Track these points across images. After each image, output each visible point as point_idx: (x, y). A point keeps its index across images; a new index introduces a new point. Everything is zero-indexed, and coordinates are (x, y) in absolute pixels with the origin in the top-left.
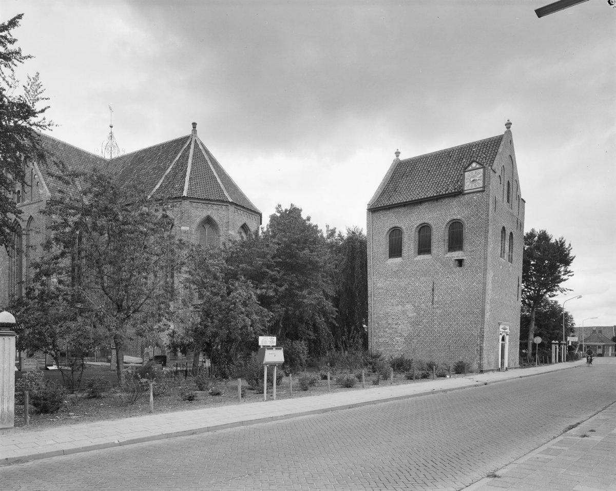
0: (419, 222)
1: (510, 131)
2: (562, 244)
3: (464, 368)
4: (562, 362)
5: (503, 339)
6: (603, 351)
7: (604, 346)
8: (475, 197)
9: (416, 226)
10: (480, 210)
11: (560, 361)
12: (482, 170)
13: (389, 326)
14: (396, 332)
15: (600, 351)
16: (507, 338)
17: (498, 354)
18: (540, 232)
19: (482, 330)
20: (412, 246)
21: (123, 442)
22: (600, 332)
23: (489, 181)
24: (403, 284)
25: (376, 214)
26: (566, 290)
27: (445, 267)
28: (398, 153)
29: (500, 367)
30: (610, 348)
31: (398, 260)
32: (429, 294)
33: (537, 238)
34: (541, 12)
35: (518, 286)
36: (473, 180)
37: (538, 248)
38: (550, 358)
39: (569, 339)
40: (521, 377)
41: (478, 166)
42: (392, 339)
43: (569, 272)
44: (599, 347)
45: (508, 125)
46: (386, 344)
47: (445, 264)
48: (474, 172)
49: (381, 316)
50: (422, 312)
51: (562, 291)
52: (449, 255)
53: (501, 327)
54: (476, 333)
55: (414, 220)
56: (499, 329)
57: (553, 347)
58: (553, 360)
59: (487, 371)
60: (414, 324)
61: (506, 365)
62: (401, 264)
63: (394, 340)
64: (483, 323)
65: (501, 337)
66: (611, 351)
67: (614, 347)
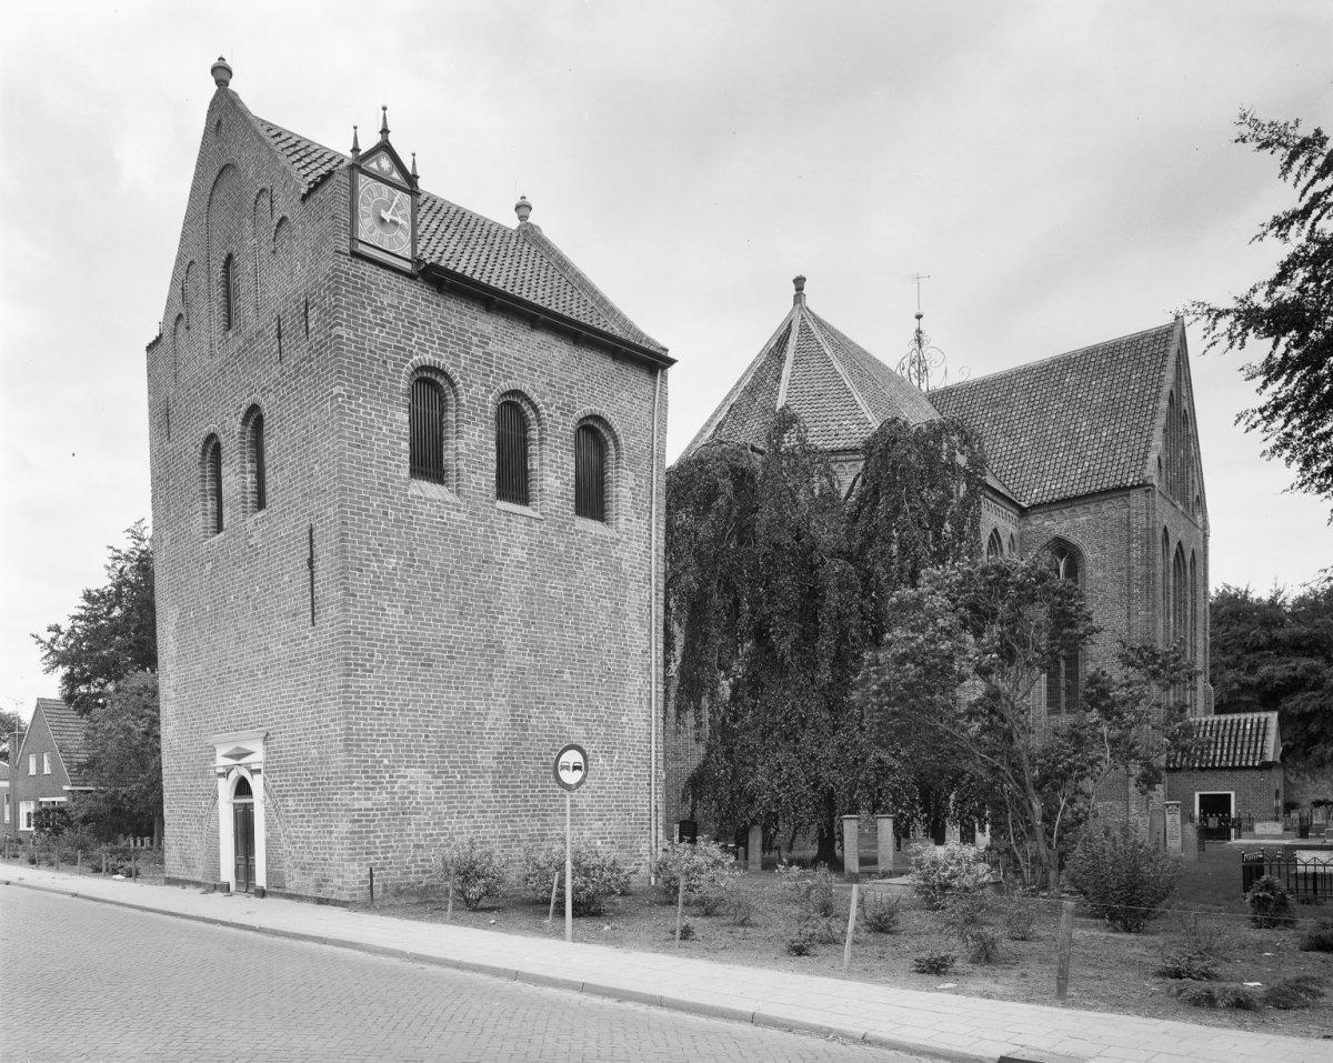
4: (563, 939)
5: (243, 788)
16: (256, 784)
29: (227, 873)
45: (222, 72)
61: (261, 880)
65: (226, 788)
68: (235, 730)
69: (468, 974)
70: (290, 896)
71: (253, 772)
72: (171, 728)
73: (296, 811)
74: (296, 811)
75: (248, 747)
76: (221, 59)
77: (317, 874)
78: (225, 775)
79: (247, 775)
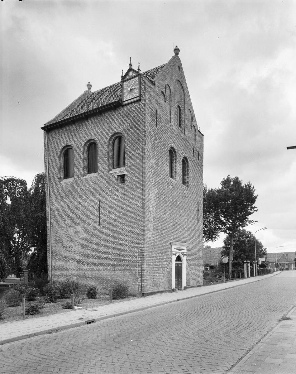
0: (87, 139)
1: (178, 59)
2: (250, 187)
3: (228, 278)
4: (254, 276)
5: (179, 259)
6: (289, 267)
7: (289, 263)
8: (133, 108)
9: (84, 143)
10: (137, 121)
11: (252, 275)
12: (137, 78)
13: (64, 249)
14: (70, 255)
15: (287, 267)
16: (184, 259)
17: (171, 275)
18: (234, 178)
19: (143, 249)
20: (81, 165)
21: (158, 304)
22: (287, 255)
23: (145, 90)
24: (74, 204)
25: (51, 134)
26: (253, 222)
27: (109, 184)
28: (89, 86)
29: (174, 286)
30: (293, 264)
31: (71, 180)
32: (96, 214)
33: (232, 183)
34: (288, 148)
35: (198, 211)
36: (131, 90)
37: (232, 190)
38: (243, 274)
39: (259, 259)
40: (178, 300)
41: (134, 75)
42: (66, 263)
43: (254, 208)
44: (287, 264)
45: (177, 50)
46: (62, 268)
47: (109, 181)
48: (131, 81)
49: (57, 238)
50: (91, 233)
51: (250, 222)
52: (113, 171)
53: (174, 247)
54: (137, 253)
55: (82, 137)
56: (171, 249)
57: (245, 265)
58: (246, 275)
59: (152, 294)
60: (85, 245)
61: (184, 284)
62: (73, 183)
63: (68, 263)
64: (143, 241)
65: (174, 258)
66: (293, 266)
67: (295, 264)
68: (178, 242)
69: (78, 328)
70: (191, 287)
71: (184, 255)
72: (150, 233)
73: (193, 266)
74: (193, 266)
75: (183, 248)
76: (176, 47)
77: (197, 280)
78: (175, 254)
79: (181, 255)
